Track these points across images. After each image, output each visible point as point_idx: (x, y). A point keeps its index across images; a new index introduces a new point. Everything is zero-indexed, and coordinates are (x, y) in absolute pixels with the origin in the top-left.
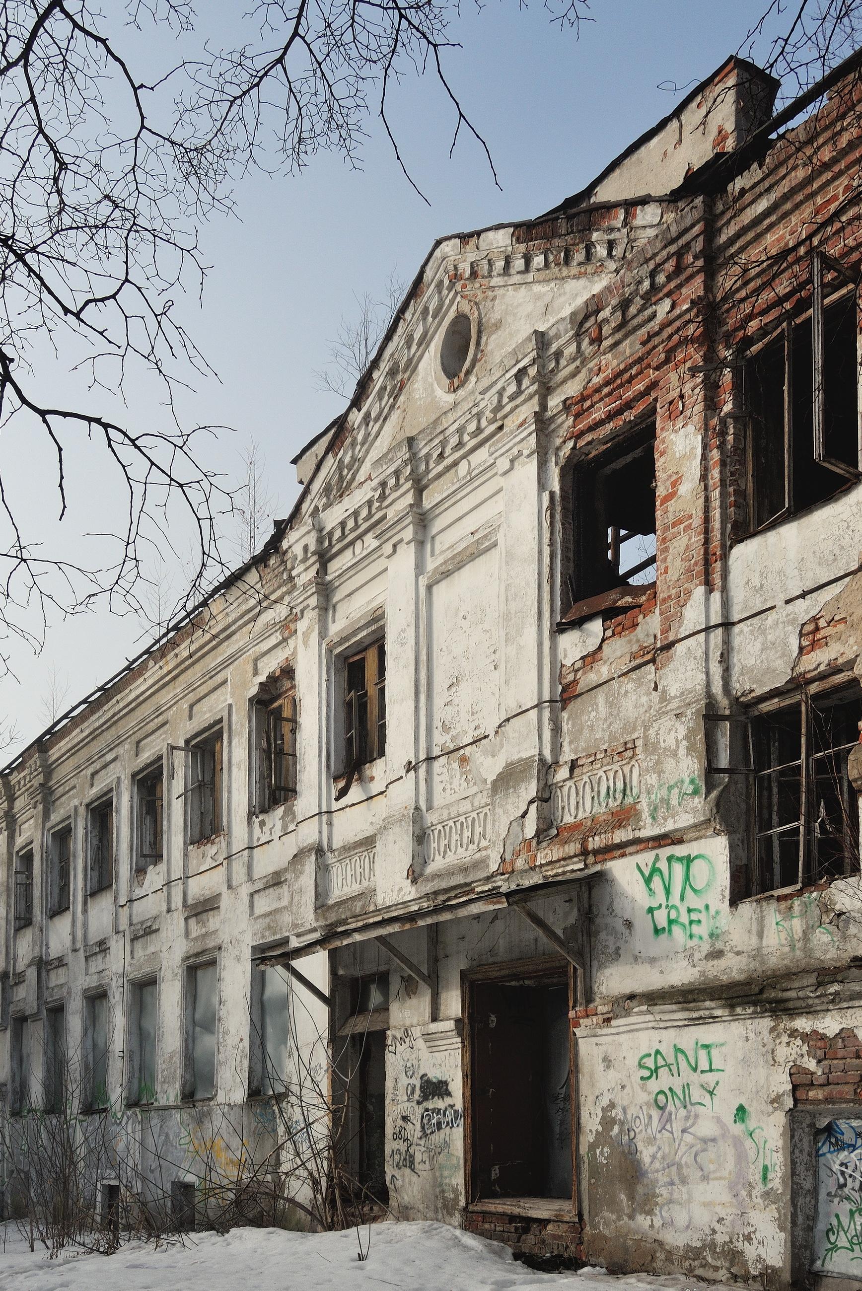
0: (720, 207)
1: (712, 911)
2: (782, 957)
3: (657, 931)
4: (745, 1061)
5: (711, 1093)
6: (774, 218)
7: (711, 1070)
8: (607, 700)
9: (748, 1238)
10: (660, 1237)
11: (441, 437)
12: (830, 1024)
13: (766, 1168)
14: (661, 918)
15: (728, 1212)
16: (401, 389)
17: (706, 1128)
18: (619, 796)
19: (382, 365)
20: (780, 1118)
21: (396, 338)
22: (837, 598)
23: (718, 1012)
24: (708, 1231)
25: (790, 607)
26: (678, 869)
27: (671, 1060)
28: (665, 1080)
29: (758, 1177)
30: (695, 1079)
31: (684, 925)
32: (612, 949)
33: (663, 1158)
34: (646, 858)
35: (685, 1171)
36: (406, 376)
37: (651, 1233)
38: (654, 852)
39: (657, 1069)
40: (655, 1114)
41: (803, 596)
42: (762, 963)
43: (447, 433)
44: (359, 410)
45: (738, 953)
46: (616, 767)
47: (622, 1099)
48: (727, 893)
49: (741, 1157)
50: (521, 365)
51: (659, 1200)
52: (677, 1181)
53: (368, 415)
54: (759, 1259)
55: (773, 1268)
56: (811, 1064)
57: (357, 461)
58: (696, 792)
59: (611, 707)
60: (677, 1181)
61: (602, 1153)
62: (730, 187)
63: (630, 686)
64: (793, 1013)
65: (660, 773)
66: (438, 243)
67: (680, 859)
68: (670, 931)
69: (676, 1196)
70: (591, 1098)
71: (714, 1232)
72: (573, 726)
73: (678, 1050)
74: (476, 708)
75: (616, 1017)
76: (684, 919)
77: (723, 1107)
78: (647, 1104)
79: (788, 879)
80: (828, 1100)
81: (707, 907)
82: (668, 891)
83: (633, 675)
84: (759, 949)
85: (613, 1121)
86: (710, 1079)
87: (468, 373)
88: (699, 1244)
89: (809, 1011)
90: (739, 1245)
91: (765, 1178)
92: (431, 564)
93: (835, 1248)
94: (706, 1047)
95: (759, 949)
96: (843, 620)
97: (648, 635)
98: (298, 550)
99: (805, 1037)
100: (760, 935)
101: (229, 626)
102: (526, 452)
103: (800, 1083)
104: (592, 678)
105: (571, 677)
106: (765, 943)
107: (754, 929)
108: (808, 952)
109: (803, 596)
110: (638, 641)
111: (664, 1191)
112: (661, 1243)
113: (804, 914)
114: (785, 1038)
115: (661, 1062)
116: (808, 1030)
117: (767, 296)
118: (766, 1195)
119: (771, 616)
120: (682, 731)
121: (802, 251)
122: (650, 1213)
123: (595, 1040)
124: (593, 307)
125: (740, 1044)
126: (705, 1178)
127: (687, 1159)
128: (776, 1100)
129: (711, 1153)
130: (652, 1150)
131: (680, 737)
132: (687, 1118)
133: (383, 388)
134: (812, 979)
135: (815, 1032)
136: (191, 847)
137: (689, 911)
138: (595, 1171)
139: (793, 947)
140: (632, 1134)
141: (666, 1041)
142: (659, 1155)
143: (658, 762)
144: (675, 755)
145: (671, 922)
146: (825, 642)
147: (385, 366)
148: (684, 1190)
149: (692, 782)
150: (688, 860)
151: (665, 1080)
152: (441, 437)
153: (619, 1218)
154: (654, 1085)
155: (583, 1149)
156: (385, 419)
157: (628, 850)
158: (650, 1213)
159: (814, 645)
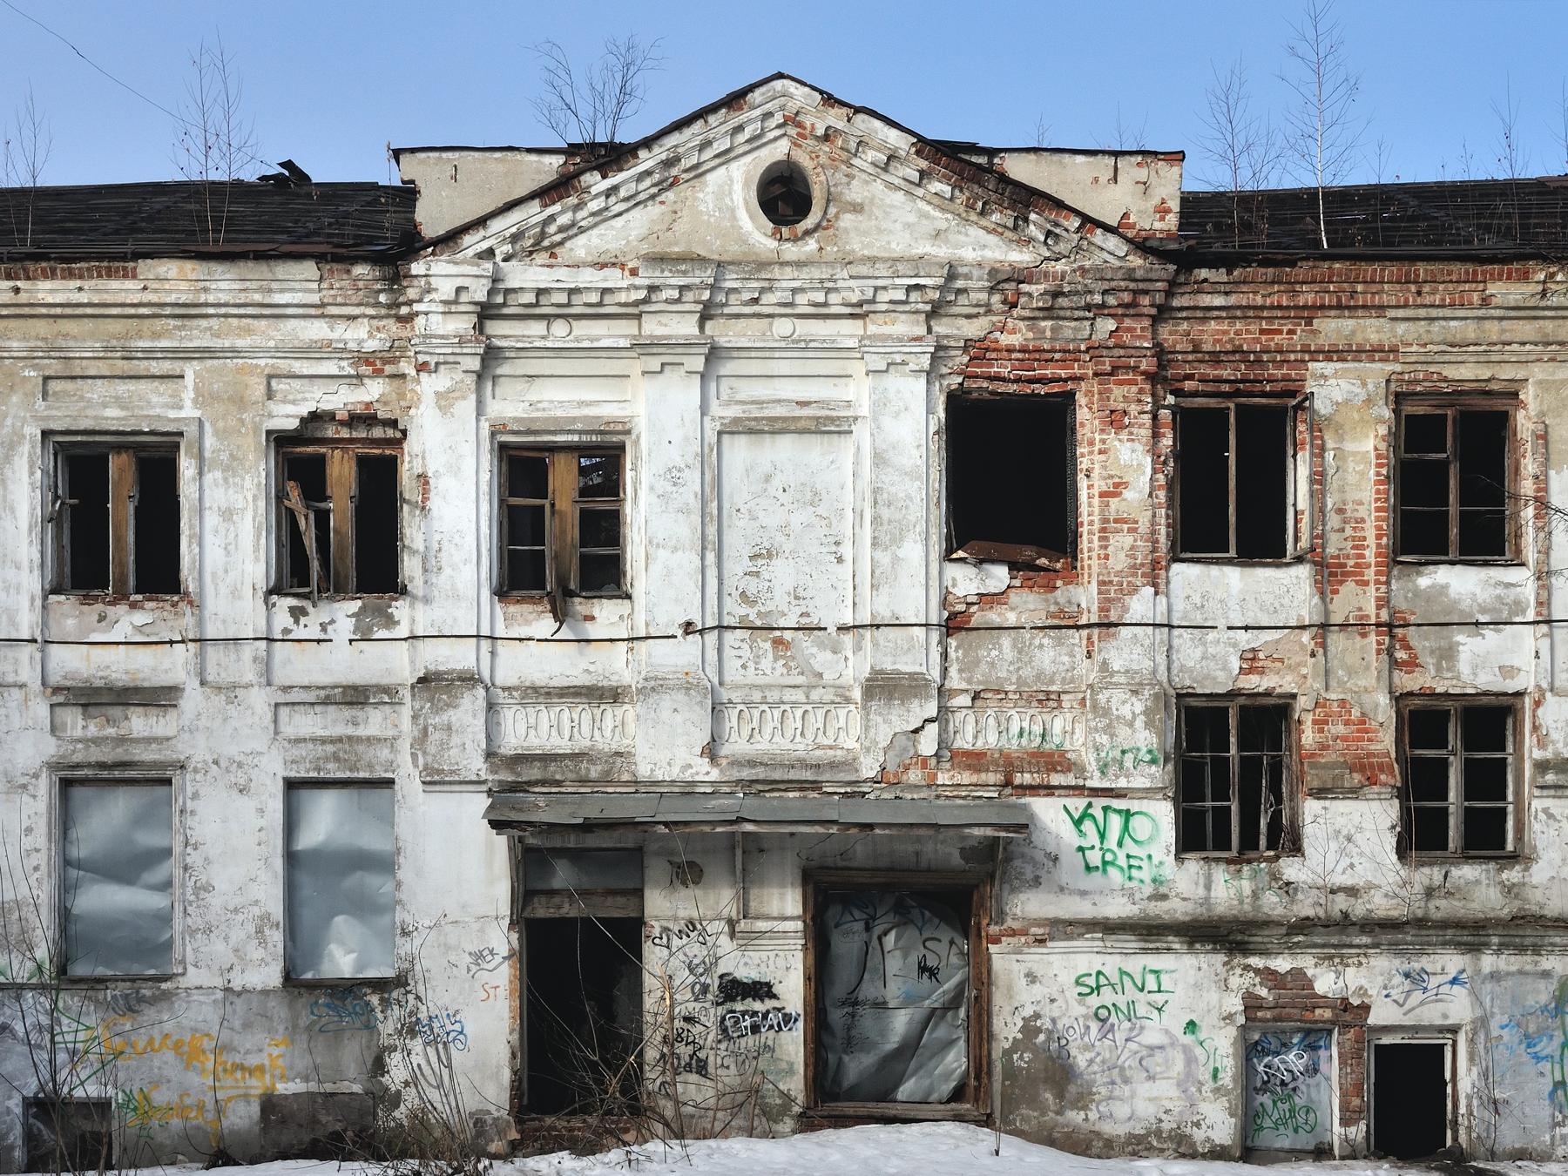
0: (1182, 279)
1: (1155, 861)
2: (1231, 908)
3: (1088, 868)
4: (1197, 986)
5: (1159, 1010)
6: (1224, 314)
7: (1159, 991)
8: (1014, 646)
9: (1197, 1125)
10: (1096, 1128)
11: (766, 284)
12: (1282, 964)
13: (1216, 1070)
14: (1094, 858)
15: (1177, 1106)
16: (672, 185)
17: (1152, 1037)
18: (1039, 740)
19: (656, 149)
20: (1232, 1032)
21: (687, 132)
22: (1278, 641)
23: (1177, 946)
24: (1153, 1121)
25: (1231, 633)
26: (1116, 822)
27: (1115, 979)
28: (1107, 996)
29: (1208, 1076)
30: (1141, 997)
31: (1122, 869)
32: (1029, 875)
33: (1103, 1062)
34: (1078, 804)
35: (1128, 1073)
36: (686, 176)
37: (1085, 1125)
38: (1087, 800)
39: (1098, 987)
40: (1094, 1026)
41: (1246, 628)
42: (1209, 910)
43: (777, 284)
44: (604, 177)
45: (1184, 899)
46: (1032, 711)
47: (1048, 1011)
48: (1173, 849)
49: (1190, 1060)
50: (922, 281)
51: (1096, 1097)
52: (1118, 1080)
53: (614, 189)
54: (1208, 1139)
55: (1222, 1146)
56: (1264, 992)
57: (573, 230)
58: (1153, 761)
59: (1020, 652)
60: (1118, 1080)
61: (1021, 1058)
62: (1196, 271)
63: (1046, 641)
64: (1253, 953)
65: (1112, 736)
66: (780, 76)
67: (1119, 812)
68: (1105, 871)
69: (1117, 1093)
70: (1008, 1009)
71: (1161, 1121)
72: (965, 656)
73: (1122, 972)
74: (801, 594)
75: (1052, 939)
76: (1122, 861)
77: (1174, 1021)
78: (1086, 1017)
79: (1223, 843)
80: (1275, 1020)
81: (1150, 857)
82: (1102, 836)
83: (1052, 633)
84: (1207, 899)
85: (1039, 1030)
86: (1159, 999)
87: (808, 233)
88: (1143, 1132)
89: (1264, 953)
90: (1188, 1131)
91: (1215, 1077)
92: (723, 411)
93: (1261, 1128)
94: (1156, 972)
95: (1207, 899)
96: (1281, 660)
97: (1069, 602)
98: (446, 289)
99: (1257, 971)
100: (1208, 887)
101: (206, 305)
102: (912, 366)
103: (1252, 1005)
104: (994, 617)
105: (962, 608)
106: (1213, 894)
107: (1202, 881)
108: (1256, 908)
109: (1246, 628)
110: (1057, 603)
111: (1103, 1091)
112: (1098, 1134)
113: (1253, 878)
114: (1238, 971)
115: (1102, 980)
116: (1261, 966)
117: (1212, 373)
118: (1217, 1090)
119: (1212, 635)
120: (1139, 708)
121: (1252, 357)
122: (1085, 1108)
123: (1019, 957)
124: (1020, 276)
125: (1192, 972)
126: (1151, 1078)
127: (1134, 1063)
128: (1229, 1017)
129: (1159, 1057)
130: (1089, 1055)
131: (1137, 711)
132: (1131, 1029)
133: (648, 173)
134: (1283, 931)
135: (1267, 968)
136: (53, 598)
137: (1128, 856)
138: (1010, 1073)
139: (1241, 902)
140: (1063, 1042)
141: (1111, 964)
142: (1098, 1060)
143: (1109, 726)
144: (1131, 724)
145: (1105, 863)
146: (1261, 671)
147: (660, 152)
148: (1127, 1088)
149: (1150, 752)
150: (1128, 814)
151: (1107, 996)
152: (766, 284)
153: (1044, 1114)
154: (1094, 1001)
155: (997, 1054)
156: (636, 205)
157: (1057, 792)
158: (1085, 1108)
159: (1251, 671)
